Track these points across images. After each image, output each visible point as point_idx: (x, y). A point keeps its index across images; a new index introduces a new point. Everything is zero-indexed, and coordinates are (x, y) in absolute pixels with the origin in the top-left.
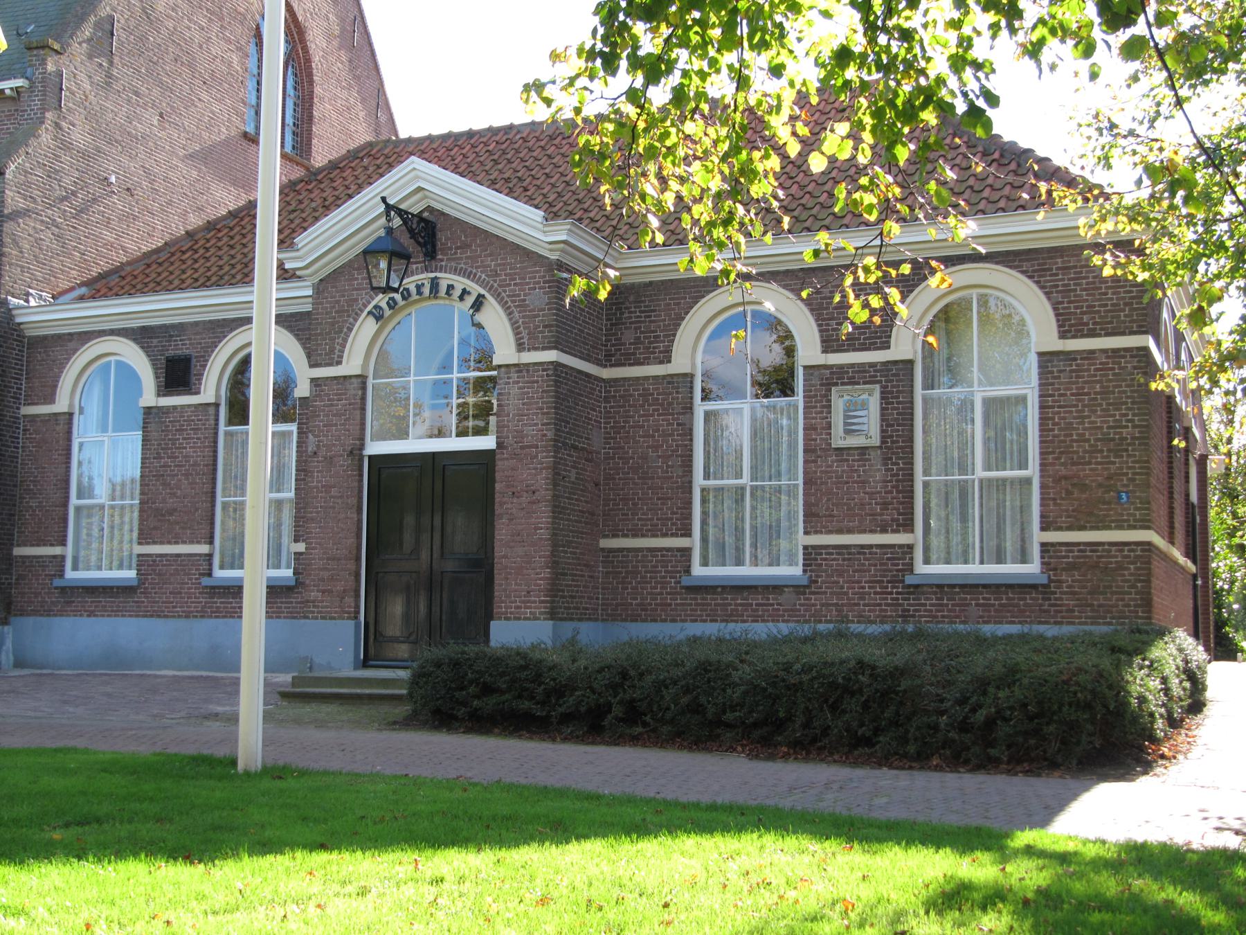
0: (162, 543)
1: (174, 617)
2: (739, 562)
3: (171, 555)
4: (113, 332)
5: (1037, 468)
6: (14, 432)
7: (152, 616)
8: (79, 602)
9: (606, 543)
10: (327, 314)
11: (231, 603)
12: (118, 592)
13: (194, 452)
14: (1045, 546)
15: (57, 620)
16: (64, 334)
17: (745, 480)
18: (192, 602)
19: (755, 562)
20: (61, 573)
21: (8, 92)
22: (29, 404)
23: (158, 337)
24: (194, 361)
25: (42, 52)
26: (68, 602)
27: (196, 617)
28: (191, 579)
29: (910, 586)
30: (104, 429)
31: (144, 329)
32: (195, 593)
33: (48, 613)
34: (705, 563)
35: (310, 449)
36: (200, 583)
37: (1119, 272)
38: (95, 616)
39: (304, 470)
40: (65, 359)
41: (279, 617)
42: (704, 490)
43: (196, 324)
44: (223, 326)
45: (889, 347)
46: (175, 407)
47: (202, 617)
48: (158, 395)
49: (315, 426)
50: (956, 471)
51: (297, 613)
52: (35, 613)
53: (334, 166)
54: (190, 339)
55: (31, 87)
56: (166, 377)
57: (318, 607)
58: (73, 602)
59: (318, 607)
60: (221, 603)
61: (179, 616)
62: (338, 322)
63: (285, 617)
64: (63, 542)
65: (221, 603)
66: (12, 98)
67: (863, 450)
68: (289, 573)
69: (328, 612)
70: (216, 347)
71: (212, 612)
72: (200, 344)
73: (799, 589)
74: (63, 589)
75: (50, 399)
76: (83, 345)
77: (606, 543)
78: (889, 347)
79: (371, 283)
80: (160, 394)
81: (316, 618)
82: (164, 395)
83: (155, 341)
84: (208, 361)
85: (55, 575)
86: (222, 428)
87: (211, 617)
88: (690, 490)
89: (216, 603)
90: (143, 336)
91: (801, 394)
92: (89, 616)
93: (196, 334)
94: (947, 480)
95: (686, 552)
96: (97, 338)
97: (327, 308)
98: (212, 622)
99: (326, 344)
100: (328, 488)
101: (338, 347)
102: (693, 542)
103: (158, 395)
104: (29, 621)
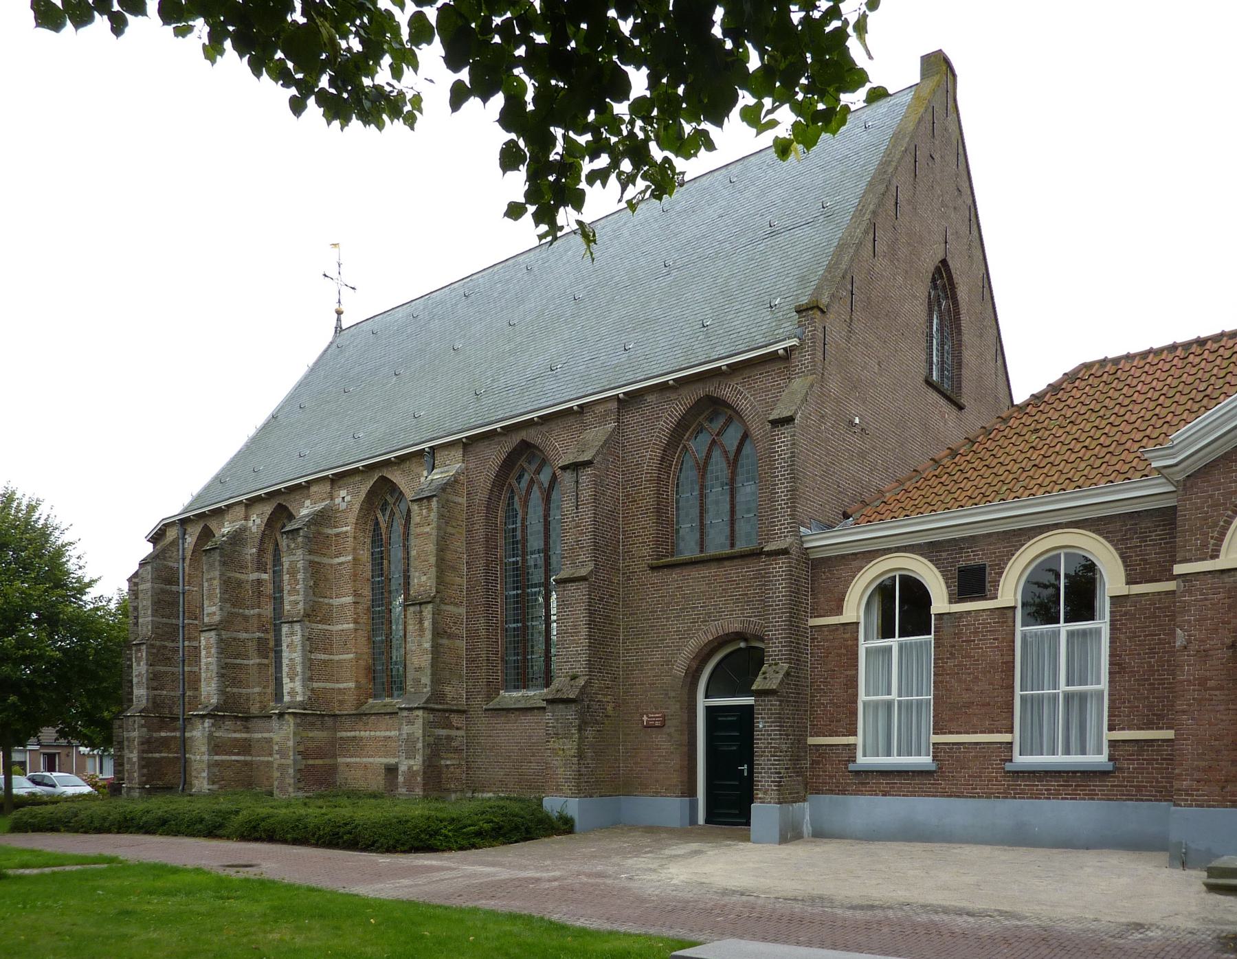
1: (974, 797)
2: (889, 753)
3: (970, 743)
4: (898, 550)
5: (1107, 684)
6: (805, 641)
8: (874, 783)
9: (812, 741)
10: (1197, 509)
11: (1038, 785)
12: (913, 776)
15: (851, 799)
16: (848, 555)
17: (894, 696)
19: (1067, 752)
20: (853, 759)
21: (575, 408)
22: (815, 617)
23: (948, 550)
24: (988, 569)
25: (810, 312)
26: (863, 783)
27: (999, 797)
28: (992, 764)
29: (1009, 772)
30: (887, 632)
31: (931, 544)
32: (996, 777)
33: (843, 792)
34: (865, 755)
35: (1178, 644)
36: (1004, 768)
38: (890, 795)
39: (1119, 664)
40: (850, 576)
41: (1093, 799)
42: (865, 704)
44: (1020, 535)
45: (996, 598)
46: (969, 612)
48: (950, 602)
49: (1184, 621)
51: (1114, 795)
52: (831, 792)
53: (1037, 399)
54: (981, 550)
55: (801, 345)
56: (959, 586)
57: (1192, 795)
58: (869, 783)
59: (1192, 795)
60: (1024, 785)
61: (979, 797)
62: (1211, 517)
63: (1098, 799)
64: (854, 733)
65: (1024, 785)
66: (577, 412)
69: (1205, 801)
70: (1013, 555)
71: (1015, 794)
72: (995, 553)
73: (1104, 774)
74: (857, 773)
75: (839, 610)
76: (868, 563)
77: (812, 741)
78: (996, 598)
80: (951, 601)
81: (1191, 806)
82: (956, 602)
83: (944, 555)
84: (1004, 568)
85: (849, 761)
86: (1019, 628)
87: (1015, 798)
88: (856, 702)
89: (1020, 785)
91: (1107, 618)
93: (990, 545)
94: (1032, 695)
95: (852, 748)
97: (1196, 503)
99: (1198, 539)
100: (1203, 682)
101: (1212, 542)
102: (1013, 737)
103: (950, 602)
104: (825, 799)
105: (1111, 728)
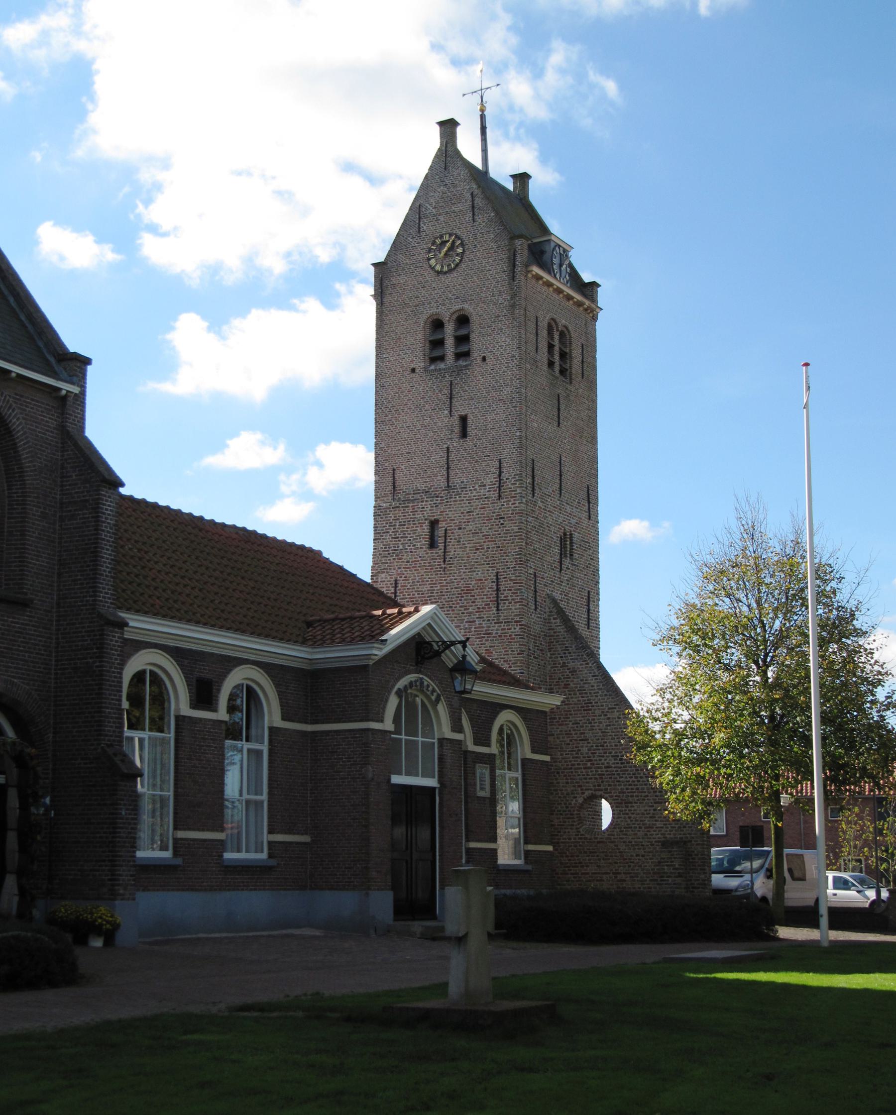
0: (194, 830)
2: (239, 851)
7: (187, 890)
13: (214, 758)
14: (270, 843)
18: (214, 878)
37: (847, 787)
43: (212, 654)
46: (201, 719)
47: (220, 890)
50: (159, 789)
60: (231, 879)
63: (268, 889)
65: (231, 879)
67: (484, 798)
68: (264, 856)
79: (455, 689)
90: (178, 654)
92: (144, 890)
96: (152, 648)
98: (227, 894)
105: (270, 832)
